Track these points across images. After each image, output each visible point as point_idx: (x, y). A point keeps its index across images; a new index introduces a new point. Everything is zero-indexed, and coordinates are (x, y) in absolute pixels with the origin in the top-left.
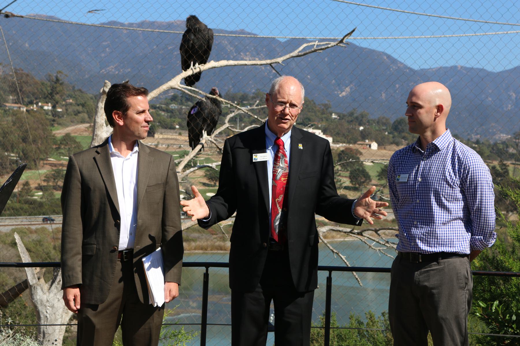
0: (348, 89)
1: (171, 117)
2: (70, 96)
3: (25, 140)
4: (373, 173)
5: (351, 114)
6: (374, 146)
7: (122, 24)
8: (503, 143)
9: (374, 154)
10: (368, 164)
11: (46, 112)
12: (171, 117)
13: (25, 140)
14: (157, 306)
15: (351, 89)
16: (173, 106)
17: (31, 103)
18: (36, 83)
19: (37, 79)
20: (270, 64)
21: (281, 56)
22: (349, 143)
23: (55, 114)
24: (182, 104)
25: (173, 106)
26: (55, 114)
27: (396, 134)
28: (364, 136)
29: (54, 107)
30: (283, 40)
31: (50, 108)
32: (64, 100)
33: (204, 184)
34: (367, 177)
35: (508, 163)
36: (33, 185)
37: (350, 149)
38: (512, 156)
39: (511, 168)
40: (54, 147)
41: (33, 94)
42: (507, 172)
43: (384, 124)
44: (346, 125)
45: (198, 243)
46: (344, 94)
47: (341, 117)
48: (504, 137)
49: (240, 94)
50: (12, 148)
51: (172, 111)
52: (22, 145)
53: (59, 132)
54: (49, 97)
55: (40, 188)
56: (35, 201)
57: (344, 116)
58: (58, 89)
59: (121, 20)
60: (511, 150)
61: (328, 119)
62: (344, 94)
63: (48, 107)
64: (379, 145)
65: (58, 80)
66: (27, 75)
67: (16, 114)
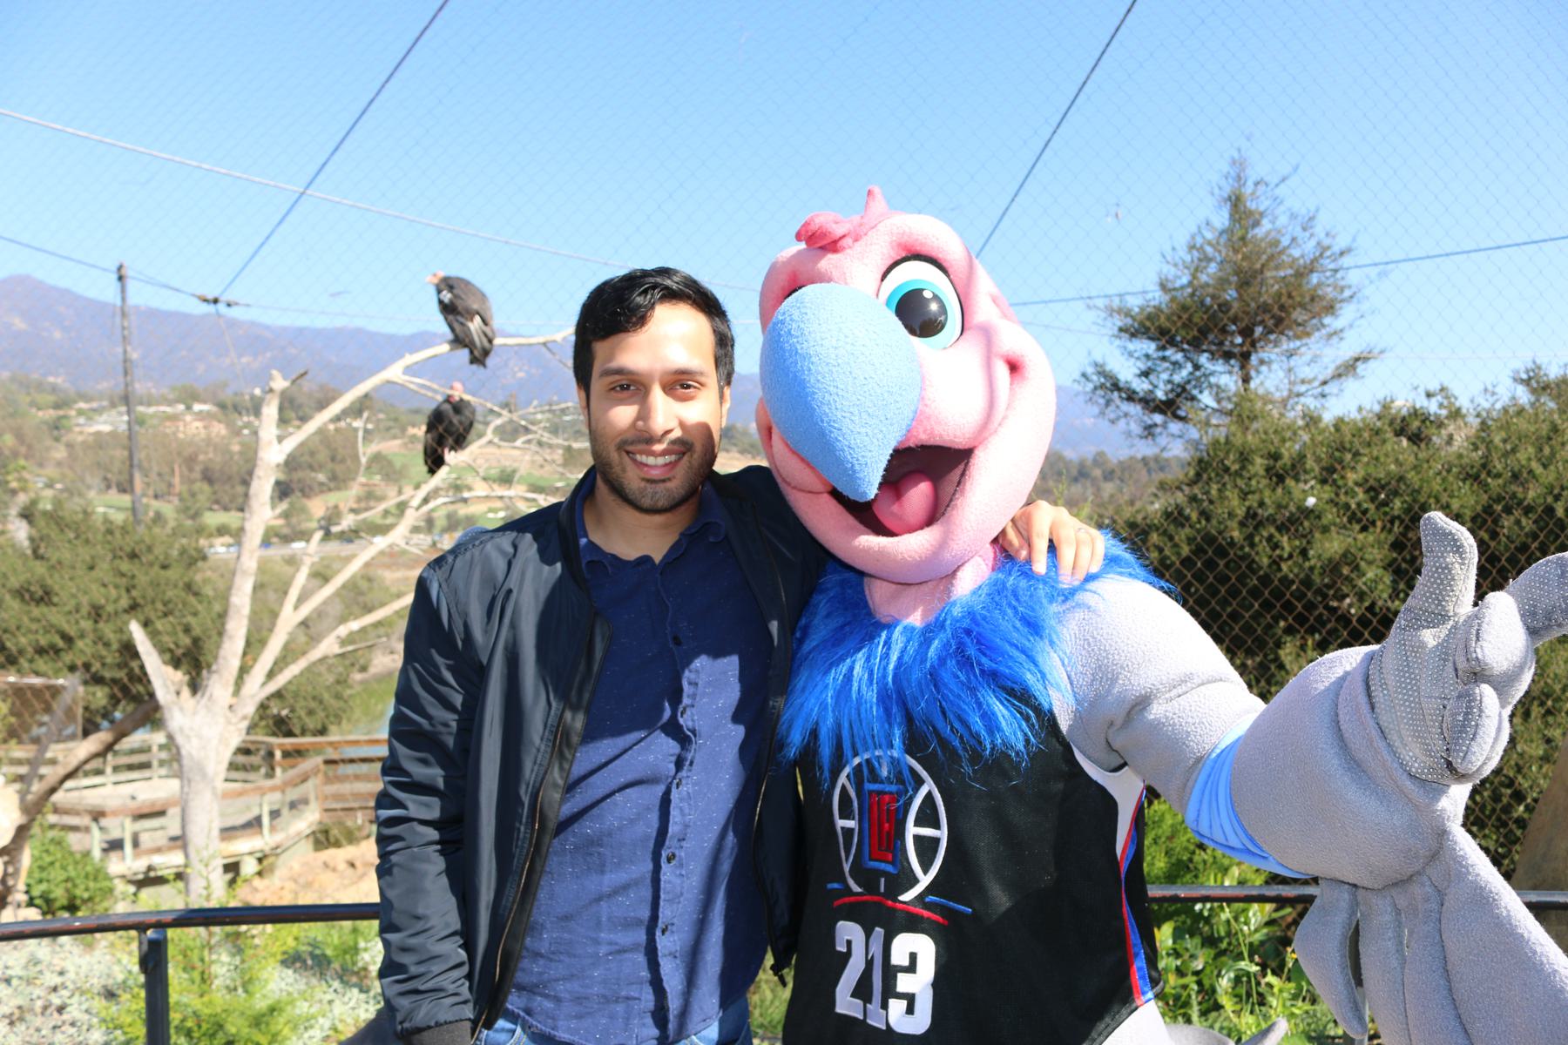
50: (321, 467)
52: (330, 465)
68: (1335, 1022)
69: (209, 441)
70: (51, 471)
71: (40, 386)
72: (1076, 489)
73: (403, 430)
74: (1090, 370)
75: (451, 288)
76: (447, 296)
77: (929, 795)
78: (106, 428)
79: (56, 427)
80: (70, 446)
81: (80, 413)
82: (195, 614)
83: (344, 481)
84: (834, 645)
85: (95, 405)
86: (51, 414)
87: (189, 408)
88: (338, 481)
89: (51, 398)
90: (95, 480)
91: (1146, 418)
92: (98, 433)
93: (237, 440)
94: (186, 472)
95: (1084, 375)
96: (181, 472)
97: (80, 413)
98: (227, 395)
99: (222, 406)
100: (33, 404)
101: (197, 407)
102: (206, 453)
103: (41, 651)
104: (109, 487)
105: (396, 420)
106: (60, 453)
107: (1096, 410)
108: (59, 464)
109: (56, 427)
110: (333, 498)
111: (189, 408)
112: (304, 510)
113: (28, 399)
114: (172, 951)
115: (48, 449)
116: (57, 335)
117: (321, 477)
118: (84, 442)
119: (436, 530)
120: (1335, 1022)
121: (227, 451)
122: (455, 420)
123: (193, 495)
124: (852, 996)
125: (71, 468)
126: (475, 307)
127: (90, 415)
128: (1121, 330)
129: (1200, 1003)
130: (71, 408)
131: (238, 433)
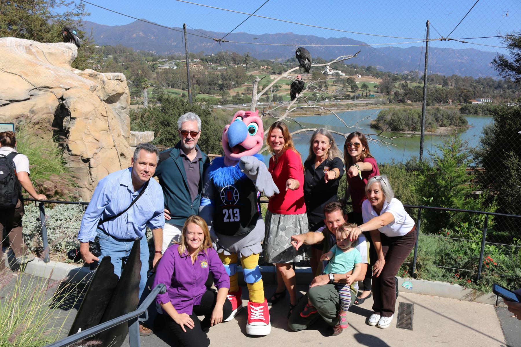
3: (237, 77)
4: (359, 86)
5: (352, 65)
6: (360, 76)
8: (406, 75)
9: (359, 79)
10: (357, 83)
11: (244, 67)
13: (237, 77)
14: (336, 315)
16: (288, 63)
17: (239, 64)
18: (240, 57)
19: (241, 55)
22: (351, 75)
23: (247, 68)
24: (291, 62)
25: (288, 63)
26: (247, 68)
28: (356, 73)
29: (247, 65)
30: (327, 38)
34: (357, 88)
35: (408, 82)
36: (240, 93)
37: (351, 78)
38: (409, 80)
39: (409, 84)
41: (239, 61)
42: (407, 85)
43: (364, 68)
44: (350, 69)
45: (297, 113)
47: (348, 66)
48: (406, 72)
50: (233, 80)
52: (236, 79)
53: (249, 74)
54: (245, 61)
55: (243, 94)
56: (241, 99)
60: (409, 77)
61: (344, 67)
63: (245, 65)
64: (362, 76)
65: (247, 56)
67: (64, 100)
69: (198, 71)
70: (152, 81)
72: (497, 92)
73: (259, 67)
74: (497, 59)
75: (300, 51)
76: (299, 53)
77: (236, 191)
78: (168, 67)
79: (153, 67)
80: (157, 73)
82: (208, 130)
83: (241, 84)
85: (164, 60)
86: (151, 63)
88: (238, 84)
89: (151, 58)
90: (164, 84)
91: (517, 76)
92: (166, 69)
93: (206, 71)
95: (495, 61)
98: (203, 56)
99: (202, 60)
100: (146, 60)
101: (194, 60)
102: (198, 75)
103: (167, 139)
104: (169, 86)
105: (257, 64)
106: (154, 75)
107: (498, 73)
108: (154, 79)
109: (153, 67)
110: (237, 90)
112: (228, 93)
113: (145, 58)
115: (151, 74)
116: (152, 38)
117: (233, 83)
119: (270, 101)
121: (204, 74)
122: (299, 86)
124: (397, 327)
125: (158, 80)
126: (307, 56)
127: (163, 63)
128: (510, 45)
129: (288, 116)
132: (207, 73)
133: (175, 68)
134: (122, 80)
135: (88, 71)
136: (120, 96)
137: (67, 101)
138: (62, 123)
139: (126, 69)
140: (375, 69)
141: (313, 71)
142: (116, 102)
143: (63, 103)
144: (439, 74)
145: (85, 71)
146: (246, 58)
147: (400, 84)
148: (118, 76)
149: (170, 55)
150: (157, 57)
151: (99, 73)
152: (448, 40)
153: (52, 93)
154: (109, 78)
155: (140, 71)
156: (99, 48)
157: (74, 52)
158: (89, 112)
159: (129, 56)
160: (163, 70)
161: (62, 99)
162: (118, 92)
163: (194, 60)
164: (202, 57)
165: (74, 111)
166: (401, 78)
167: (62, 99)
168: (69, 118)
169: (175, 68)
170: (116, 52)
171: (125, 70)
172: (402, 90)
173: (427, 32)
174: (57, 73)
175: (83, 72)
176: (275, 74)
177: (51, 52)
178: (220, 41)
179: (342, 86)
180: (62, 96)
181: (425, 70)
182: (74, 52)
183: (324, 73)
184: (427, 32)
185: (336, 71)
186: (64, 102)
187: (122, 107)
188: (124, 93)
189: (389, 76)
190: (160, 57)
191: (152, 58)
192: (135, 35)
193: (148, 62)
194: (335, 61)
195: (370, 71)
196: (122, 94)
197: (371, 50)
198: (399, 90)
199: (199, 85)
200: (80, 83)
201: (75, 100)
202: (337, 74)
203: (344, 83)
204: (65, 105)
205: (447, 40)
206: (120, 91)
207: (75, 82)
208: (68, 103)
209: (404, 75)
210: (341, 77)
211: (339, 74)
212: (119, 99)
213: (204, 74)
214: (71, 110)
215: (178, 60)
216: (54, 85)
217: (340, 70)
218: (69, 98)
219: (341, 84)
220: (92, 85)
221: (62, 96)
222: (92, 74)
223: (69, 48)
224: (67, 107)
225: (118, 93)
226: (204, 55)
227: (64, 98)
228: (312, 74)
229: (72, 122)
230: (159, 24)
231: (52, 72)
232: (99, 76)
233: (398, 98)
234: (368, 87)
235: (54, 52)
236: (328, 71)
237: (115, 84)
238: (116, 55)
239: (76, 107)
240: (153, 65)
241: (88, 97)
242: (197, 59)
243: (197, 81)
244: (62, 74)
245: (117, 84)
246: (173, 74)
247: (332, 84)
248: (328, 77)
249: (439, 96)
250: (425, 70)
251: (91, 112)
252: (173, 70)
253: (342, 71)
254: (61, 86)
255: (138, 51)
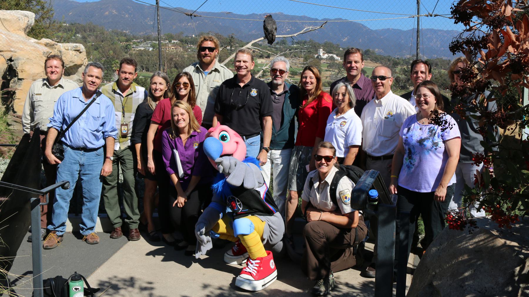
0: (346, 38)
1: (276, 50)
2: (237, 43)
7: (257, 15)
8: (408, 59)
11: (228, 50)
12: (276, 50)
15: (348, 38)
20: (291, 37)
21: (295, 33)
23: (231, 50)
26: (231, 50)
27: (366, 56)
29: (231, 47)
31: (229, 48)
32: (235, 45)
33: (290, 77)
40: (231, 63)
46: (345, 40)
48: (408, 56)
49: (303, 41)
51: (277, 48)
57: (345, 49)
58: (232, 41)
59: (256, 13)
62: (345, 40)
63: (229, 48)
65: (232, 37)
66: (221, 36)
68: (492, 269)
71: (122, 34)
78: (142, 49)
81: (134, 43)
84: (268, 191)
85: (139, 41)
86: (124, 44)
87: (170, 42)
89: (124, 38)
92: (140, 50)
93: (186, 53)
94: (169, 65)
96: (167, 64)
97: (134, 43)
98: (183, 37)
99: (181, 41)
100: (119, 40)
101: (173, 41)
109: (127, 48)
111: (170, 42)
113: (117, 38)
114: (32, 287)
116: (127, 16)
118: (135, 53)
120: (492, 269)
121: (183, 57)
123: (172, 73)
127: (137, 44)
130: (131, 42)
131: (187, 51)
132: (186, 56)
133: (151, 49)
134: (81, 51)
135: (45, 40)
136: (78, 68)
137: (15, 62)
138: (9, 84)
139: (95, 50)
140: (373, 53)
141: (304, 55)
142: (75, 74)
143: (11, 65)
144: (444, 58)
145: (41, 40)
146: (230, 40)
147: (401, 69)
148: (77, 47)
149: (146, 35)
150: (132, 37)
151: (56, 43)
152: (435, 16)
153: (2, 55)
154: (66, 48)
155: (111, 52)
156: (66, 26)
157: (30, 21)
158: (38, 74)
159: (99, 35)
160: (138, 52)
161: (11, 60)
162: (76, 63)
163: (173, 41)
164: (182, 38)
165: (22, 72)
166: (402, 63)
167: (11, 60)
168: (16, 79)
169: (151, 49)
170: (85, 31)
171: (95, 51)
172: (403, 76)
173: (418, 9)
174: (9, 37)
175: (40, 41)
176: (263, 58)
177: (5, 18)
178: (191, 15)
179: (336, 71)
180: (11, 58)
181: (417, 49)
182: (30, 21)
183: (318, 57)
184: (418, 9)
185: (331, 55)
186: (12, 63)
187: (80, 80)
188: (82, 65)
189: (389, 60)
190: (135, 38)
191: (125, 38)
192: (107, 13)
193: (121, 42)
194: (302, 32)
195: (368, 54)
196: (80, 66)
197: (369, 32)
198: (400, 76)
199: (177, 69)
200: (32, 48)
201: (23, 61)
202: (332, 58)
203: (339, 68)
204: (13, 66)
205: (433, 16)
206: (78, 62)
207: (27, 47)
208: (16, 64)
209: (405, 59)
210: (336, 62)
211: (334, 58)
212: (77, 71)
213: (184, 57)
214: (18, 70)
215: (154, 40)
216: (5, 49)
217: (334, 54)
218: (18, 59)
219: (336, 69)
220: (45, 51)
221: (11, 58)
222: (48, 44)
223: (26, 16)
224: (15, 68)
225: (76, 65)
226: (184, 35)
227: (13, 59)
228: (304, 57)
229: (19, 83)
230: (361, 141)
231: (4, 36)
232: (55, 46)
233: (399, 85)
234: (366, 73)
235: (9, 18)
236: (321, 54)
237: (73, 55)
238: (85, 35)
239: (24, 68)
240: (126, 46)
241: (38, 59)
242: (176, 40)
243: (175, 64)
244: (14, 39)
245: (75, 55)
246: (149, 56)
247: (326, 69)
248: (322, 62)
249: (444, 82)
250: (417, 49)
251: (39, 73)
252: (149, 52)
253: (337, 56)
254: (12, 49)
255: (110, 30)
